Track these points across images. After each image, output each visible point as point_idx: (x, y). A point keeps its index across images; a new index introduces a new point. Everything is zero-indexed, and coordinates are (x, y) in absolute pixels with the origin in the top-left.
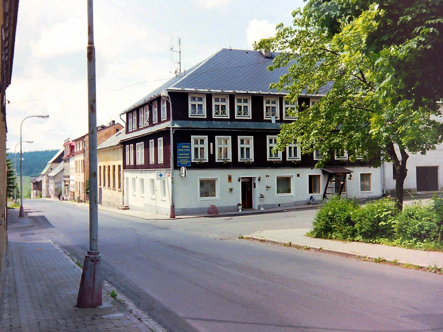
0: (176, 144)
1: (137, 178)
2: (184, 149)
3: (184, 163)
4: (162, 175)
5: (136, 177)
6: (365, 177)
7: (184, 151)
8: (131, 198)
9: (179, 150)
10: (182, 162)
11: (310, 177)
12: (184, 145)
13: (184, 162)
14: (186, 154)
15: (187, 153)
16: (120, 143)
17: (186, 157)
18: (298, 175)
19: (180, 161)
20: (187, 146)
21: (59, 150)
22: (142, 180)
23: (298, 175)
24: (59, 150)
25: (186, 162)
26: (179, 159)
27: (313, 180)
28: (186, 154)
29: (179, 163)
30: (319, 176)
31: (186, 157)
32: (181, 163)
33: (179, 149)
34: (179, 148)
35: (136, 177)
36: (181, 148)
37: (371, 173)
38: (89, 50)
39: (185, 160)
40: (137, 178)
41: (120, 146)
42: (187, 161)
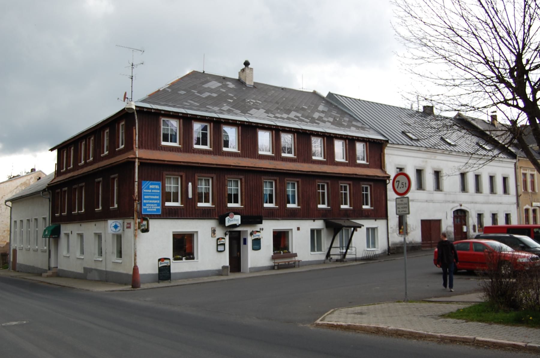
0: (141, 183)
1: (72, 233)
2: (152, 189)
3: (152, 210)
4: (117, 228)
5: (72, 232)
6: (372, 231)
7: (151, 192)
8: (61, 259)
9: (145, 191)
10: (149, 208)
11: (312, 231)
12: (151, 184)
13: (151, 208)
14: (155, 197)
15: (157, 195)
16: (48, 187)
17: (154, 201)
18: (298, 229)
19: (146, 206)
20: (157, 186)
21: (49, 150)
22: (81, 236)
23: (298, 229)
24: (49, 150)
25: (153, 208)
26: (144, 203)
27: (315, 234)
28: (155, 197)
29: (144, 209)
30: (195, 144)
31: (154, 201)
32: (146, 209)
33: (145, 189)
34: (144, 188)
35: (72, 232)
36: (148, 188)
37: (377, 228)
38: (336, 163)
39: (152, 205)
40: (72, 233)
41: (47, 193)
42: (155, 206)
